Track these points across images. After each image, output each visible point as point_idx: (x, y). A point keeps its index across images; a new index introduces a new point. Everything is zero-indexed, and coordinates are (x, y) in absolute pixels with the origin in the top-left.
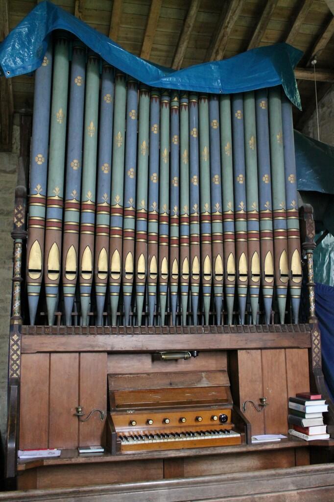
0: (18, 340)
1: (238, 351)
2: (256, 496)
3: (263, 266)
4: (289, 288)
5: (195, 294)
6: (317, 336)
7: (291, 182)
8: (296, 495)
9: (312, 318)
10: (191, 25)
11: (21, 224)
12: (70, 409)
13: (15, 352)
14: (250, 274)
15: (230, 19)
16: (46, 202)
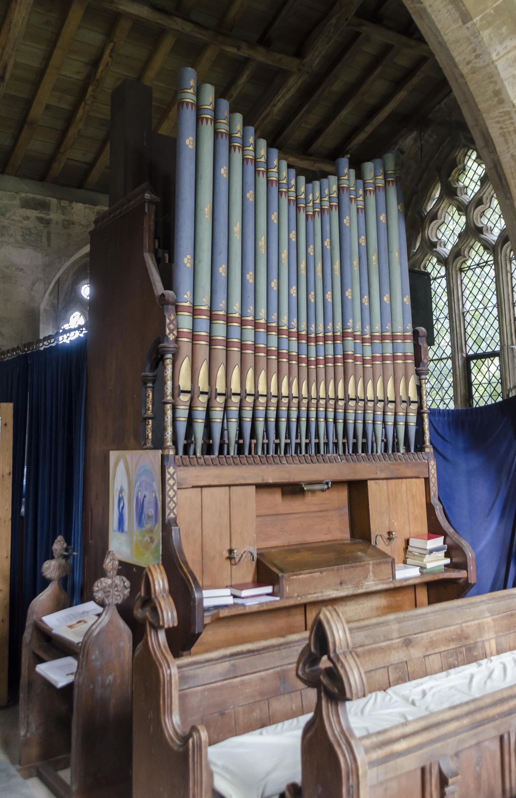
0: (174, 473)
1: (368, 481)
2: (463, 625)
3: (336, 390)
4: (209, 409)
5: (390, 423)
6: (434, 465)
7: (407, 303)
8: (491, 621)
9: (427, 447)
10: (234, 96)
11: (174, 337)
12: (223, 552)
13: (172, 487)
14: (301, 397)
15: (281, 97)
16: (195, 312)
